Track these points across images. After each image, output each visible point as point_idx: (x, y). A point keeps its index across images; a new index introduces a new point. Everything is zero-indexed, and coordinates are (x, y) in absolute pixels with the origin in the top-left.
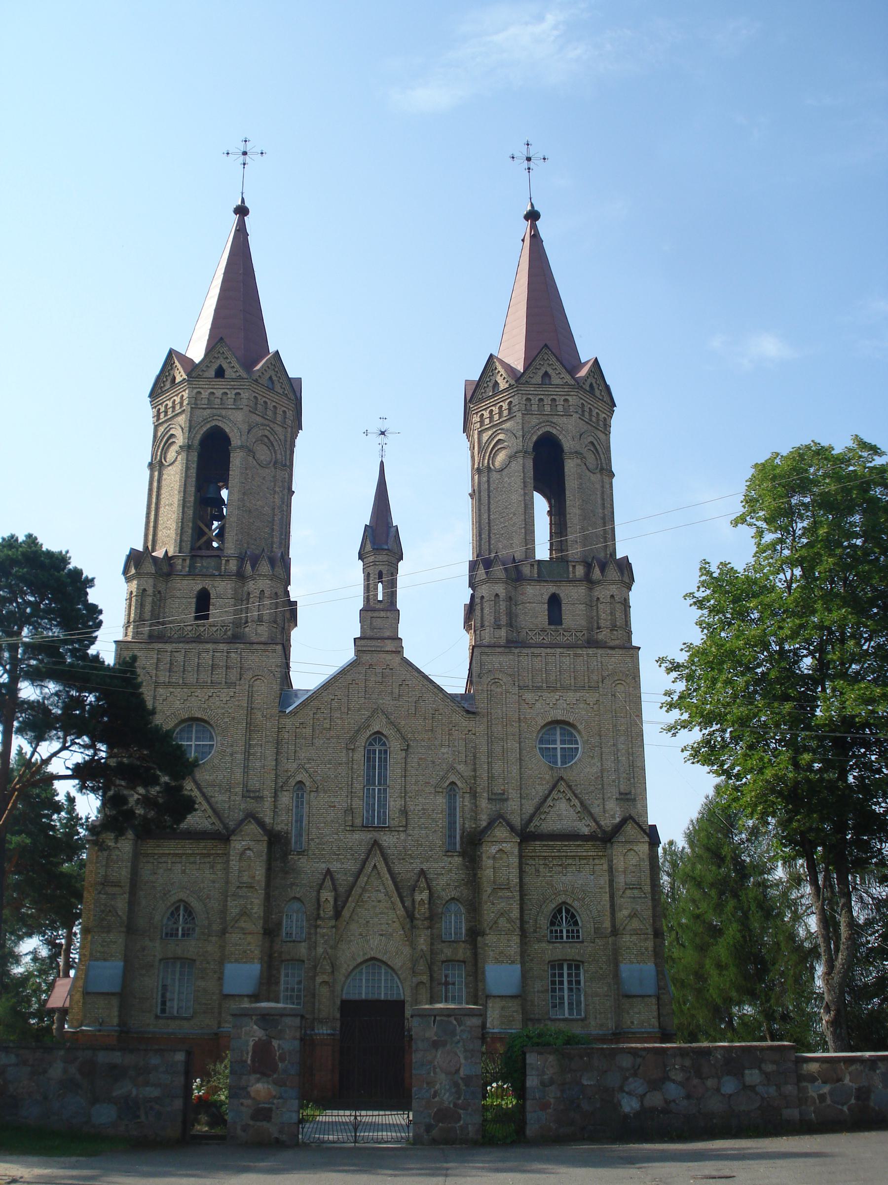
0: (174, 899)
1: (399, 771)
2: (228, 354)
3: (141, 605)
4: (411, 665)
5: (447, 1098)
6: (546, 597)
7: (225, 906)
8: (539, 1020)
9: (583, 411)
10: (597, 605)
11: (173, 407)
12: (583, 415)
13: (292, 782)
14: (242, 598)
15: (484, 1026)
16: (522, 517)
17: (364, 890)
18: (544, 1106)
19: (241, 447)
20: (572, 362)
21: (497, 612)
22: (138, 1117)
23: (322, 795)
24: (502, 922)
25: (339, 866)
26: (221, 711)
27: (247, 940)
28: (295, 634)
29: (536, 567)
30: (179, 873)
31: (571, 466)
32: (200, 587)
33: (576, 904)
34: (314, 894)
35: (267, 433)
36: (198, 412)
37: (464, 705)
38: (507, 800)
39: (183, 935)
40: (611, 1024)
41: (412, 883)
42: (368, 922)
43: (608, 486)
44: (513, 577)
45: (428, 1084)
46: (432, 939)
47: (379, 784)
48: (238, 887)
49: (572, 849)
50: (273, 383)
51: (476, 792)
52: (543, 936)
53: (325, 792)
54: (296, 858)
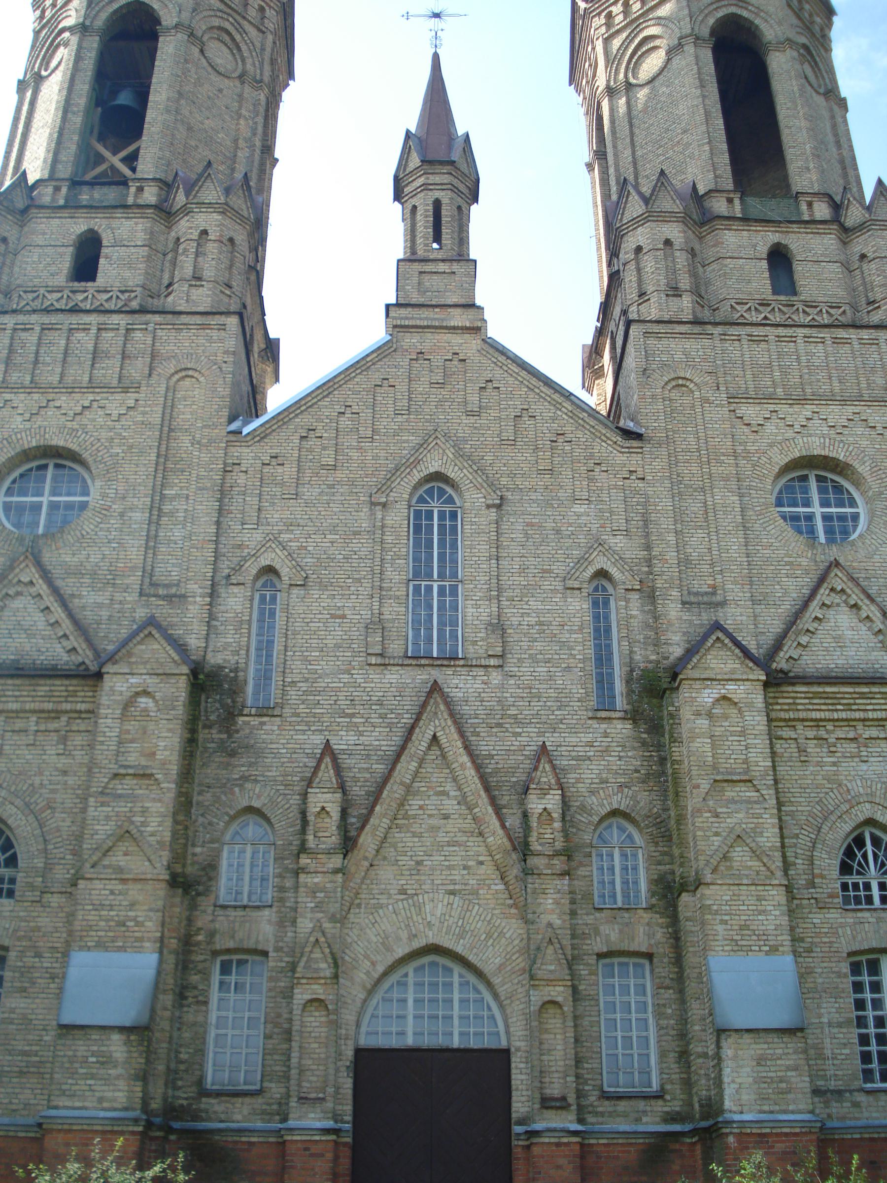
1: (483, 549)
4: (502, 351)
6: (763, 250)
7: (83, 825)
8: (839, 1093)
10: (860, 267)
13: (252, 568)
14: (162, 253)
16: (704, 128)
23: (315, 593)
24: (740, 855)
25: (352, 738)
26: (104, 434)
34: (295, 800)
38: (723, 604)
42: (419, 863)
46: (573, 902)
47: (442, 576)
48: (116, 775)
51: (653, 589)
53: (323, 587)
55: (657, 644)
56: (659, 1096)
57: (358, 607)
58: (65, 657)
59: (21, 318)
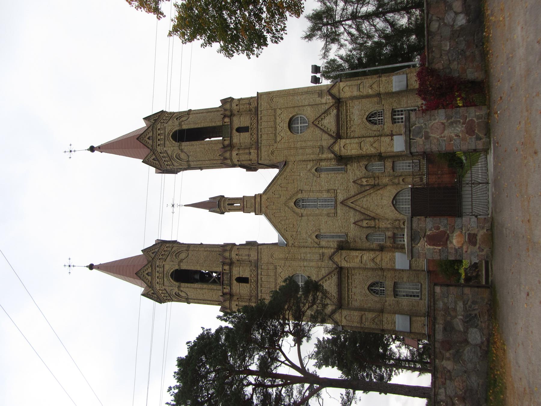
0: (368, 292)
5: (459, 129)
6: (238, 134)
13: (316, 240)
17: (362, 207)
23: (321, 227)
27: (384, 259)
28: (259, 242)
32: (235, 281)
33: (367, 114)
34: (364, 229)
41: (359, 186)
45: (451, 141)
53: (320, 226)
55: (331, 159)
56: (420, 160)
59: (259, 292)
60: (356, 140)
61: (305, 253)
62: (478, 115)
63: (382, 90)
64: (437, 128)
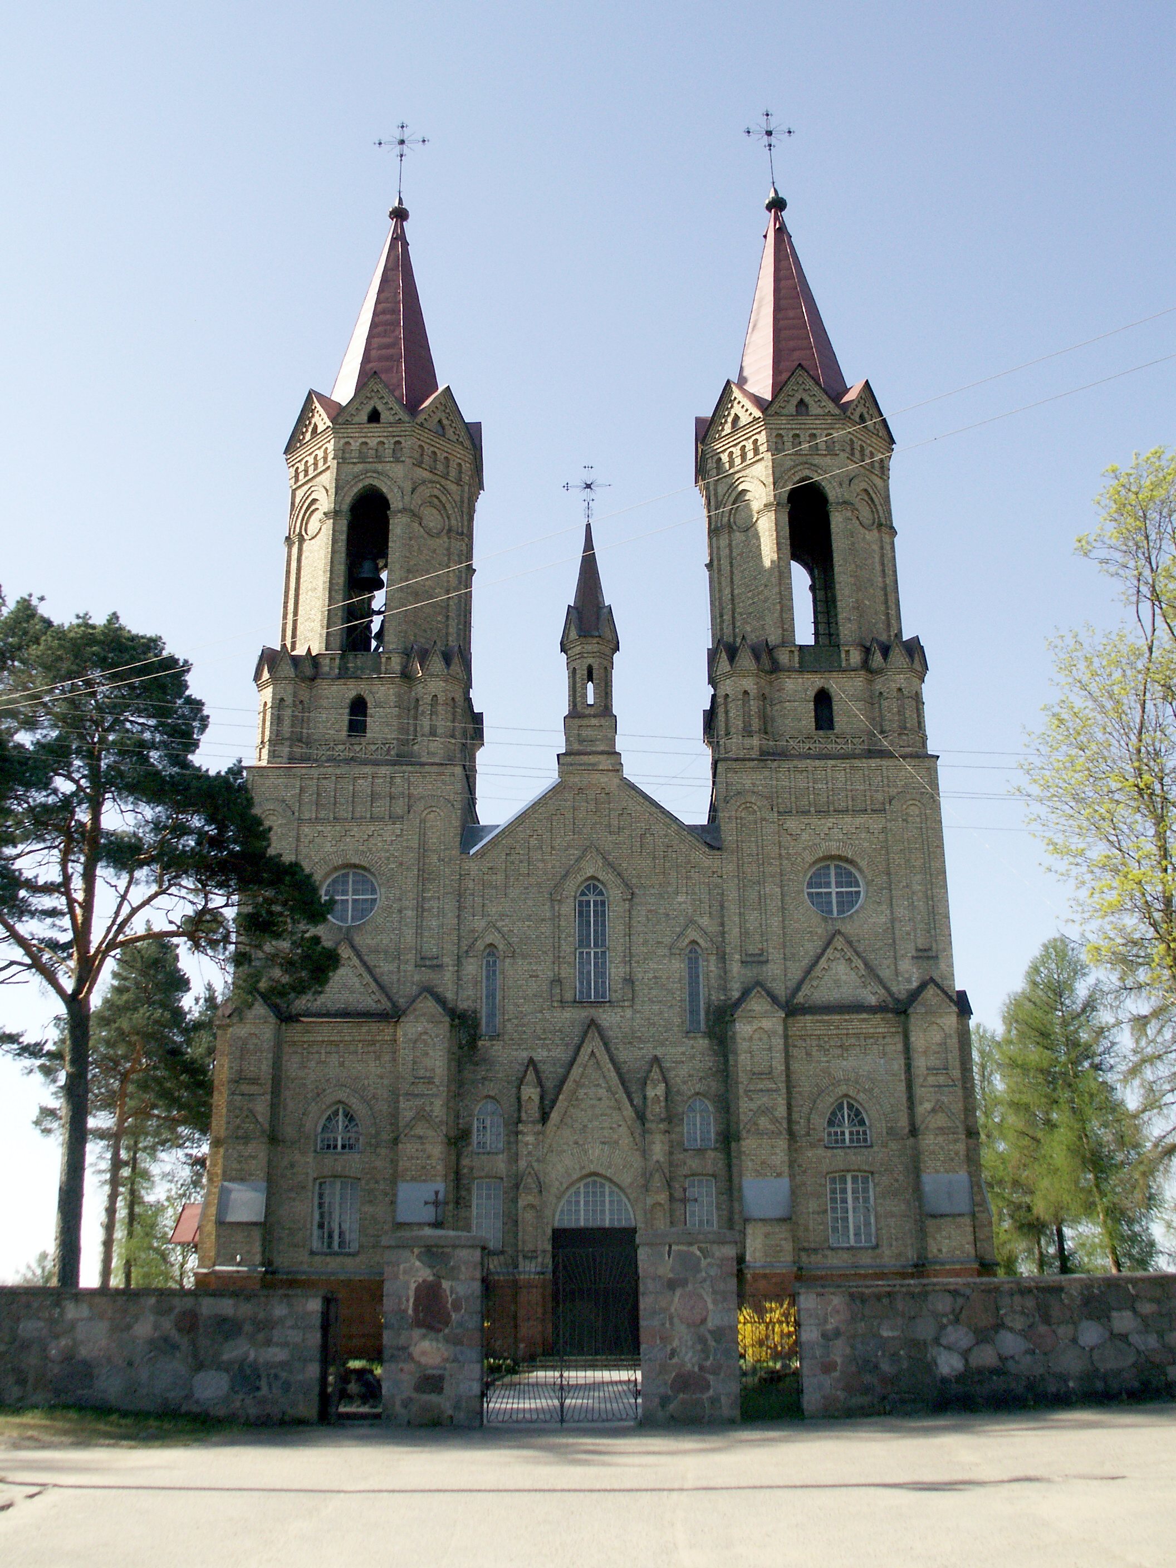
0: (329, 1100)
2: (384, 392)
3: (277, 720)
4: (633, 787)
5: (689, 1359)
6: (811, 693)
8: (815, 1250)
9: (853, 449)
11: (316, 464)
12: (853, 454)
13: (480, 945)
14: (410, 708)
15: (741, 1259)
17: (578, 1084)
18: (828, 1368)
19: (404, 510)
20: (836, 388)
21: (746, 715)
22: (258, 1389)
25: (545, 1054)
28: (482, 756)
29: (796, 653)
30: (335, 1066)
31: (837, 520)
32: (353, 694)
33: (861, 1097)
34: (514, 1090)
35: (436, 492)
36: (348, 468)
37: (710, 836)
39: (344, 1147)
40: (911, 1255)
42: (585, 1126)
43: (888, 547)
44: (767, 667)
47: (596, 945)
49: (856, 1023)
50: (443, 428)
52: (819, 1140)
53: (524, 957)
54: (488, 1044)
57: (546, 971)
58: (374, 1005)
60: (779, 1067)
61: (441, 913)
62: (718, 1400)
63: (929, 1141)
64: (693, 1307)
